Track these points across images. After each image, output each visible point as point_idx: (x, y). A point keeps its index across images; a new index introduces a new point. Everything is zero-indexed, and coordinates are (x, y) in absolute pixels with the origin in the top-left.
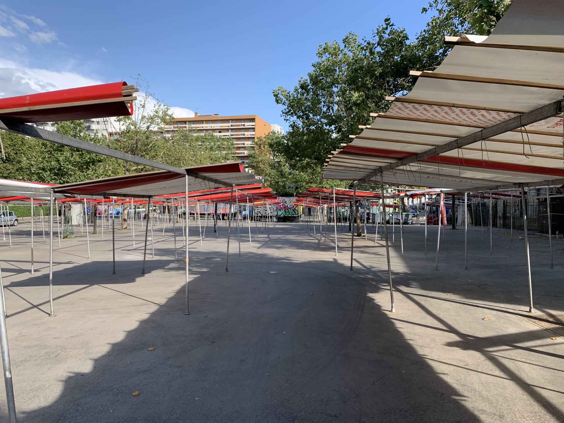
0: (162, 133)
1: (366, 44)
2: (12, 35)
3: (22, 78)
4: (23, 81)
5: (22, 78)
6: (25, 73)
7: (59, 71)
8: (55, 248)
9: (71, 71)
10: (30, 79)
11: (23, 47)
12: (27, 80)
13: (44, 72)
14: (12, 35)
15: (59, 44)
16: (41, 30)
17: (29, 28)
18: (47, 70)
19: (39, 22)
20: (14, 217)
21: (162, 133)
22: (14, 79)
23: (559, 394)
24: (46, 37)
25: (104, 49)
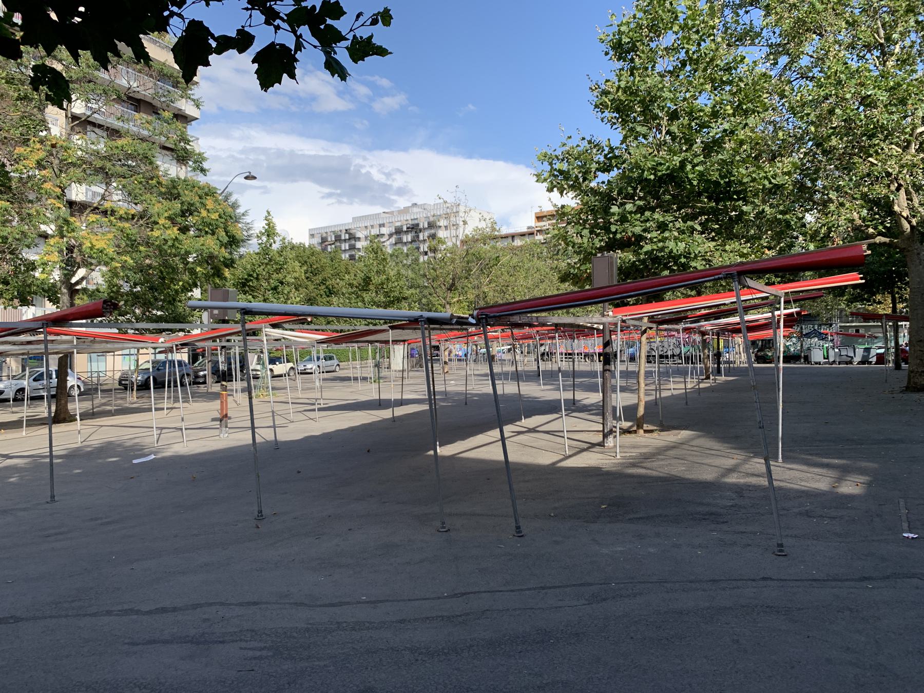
0: (533, 234)
1: (585, 143)
2: (351, 106)
3: (362, 166)
4: (363, 171)
5: (362, 166)
6: (365, 159)
7: (405, 149)
8: (158, 406)
9: (421, 147)
10: (371, 166)
11: (365, 122)
12: (368, 169)
13: (386, 154)
14: (351, 106)
15: (410, 109)
16: (386, 93)
17: (371, 93)
18: (391, 150)
19: (385, 83)
20: (335, 362)
21: (533, 234)
22: (352, 169)
23: (48, 475)
24: (392, 102)
25: (471, 107)
